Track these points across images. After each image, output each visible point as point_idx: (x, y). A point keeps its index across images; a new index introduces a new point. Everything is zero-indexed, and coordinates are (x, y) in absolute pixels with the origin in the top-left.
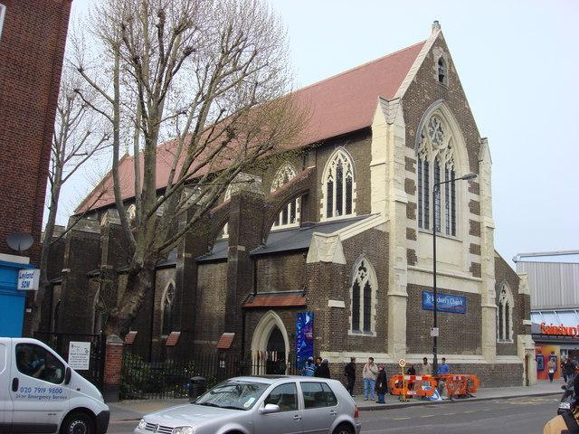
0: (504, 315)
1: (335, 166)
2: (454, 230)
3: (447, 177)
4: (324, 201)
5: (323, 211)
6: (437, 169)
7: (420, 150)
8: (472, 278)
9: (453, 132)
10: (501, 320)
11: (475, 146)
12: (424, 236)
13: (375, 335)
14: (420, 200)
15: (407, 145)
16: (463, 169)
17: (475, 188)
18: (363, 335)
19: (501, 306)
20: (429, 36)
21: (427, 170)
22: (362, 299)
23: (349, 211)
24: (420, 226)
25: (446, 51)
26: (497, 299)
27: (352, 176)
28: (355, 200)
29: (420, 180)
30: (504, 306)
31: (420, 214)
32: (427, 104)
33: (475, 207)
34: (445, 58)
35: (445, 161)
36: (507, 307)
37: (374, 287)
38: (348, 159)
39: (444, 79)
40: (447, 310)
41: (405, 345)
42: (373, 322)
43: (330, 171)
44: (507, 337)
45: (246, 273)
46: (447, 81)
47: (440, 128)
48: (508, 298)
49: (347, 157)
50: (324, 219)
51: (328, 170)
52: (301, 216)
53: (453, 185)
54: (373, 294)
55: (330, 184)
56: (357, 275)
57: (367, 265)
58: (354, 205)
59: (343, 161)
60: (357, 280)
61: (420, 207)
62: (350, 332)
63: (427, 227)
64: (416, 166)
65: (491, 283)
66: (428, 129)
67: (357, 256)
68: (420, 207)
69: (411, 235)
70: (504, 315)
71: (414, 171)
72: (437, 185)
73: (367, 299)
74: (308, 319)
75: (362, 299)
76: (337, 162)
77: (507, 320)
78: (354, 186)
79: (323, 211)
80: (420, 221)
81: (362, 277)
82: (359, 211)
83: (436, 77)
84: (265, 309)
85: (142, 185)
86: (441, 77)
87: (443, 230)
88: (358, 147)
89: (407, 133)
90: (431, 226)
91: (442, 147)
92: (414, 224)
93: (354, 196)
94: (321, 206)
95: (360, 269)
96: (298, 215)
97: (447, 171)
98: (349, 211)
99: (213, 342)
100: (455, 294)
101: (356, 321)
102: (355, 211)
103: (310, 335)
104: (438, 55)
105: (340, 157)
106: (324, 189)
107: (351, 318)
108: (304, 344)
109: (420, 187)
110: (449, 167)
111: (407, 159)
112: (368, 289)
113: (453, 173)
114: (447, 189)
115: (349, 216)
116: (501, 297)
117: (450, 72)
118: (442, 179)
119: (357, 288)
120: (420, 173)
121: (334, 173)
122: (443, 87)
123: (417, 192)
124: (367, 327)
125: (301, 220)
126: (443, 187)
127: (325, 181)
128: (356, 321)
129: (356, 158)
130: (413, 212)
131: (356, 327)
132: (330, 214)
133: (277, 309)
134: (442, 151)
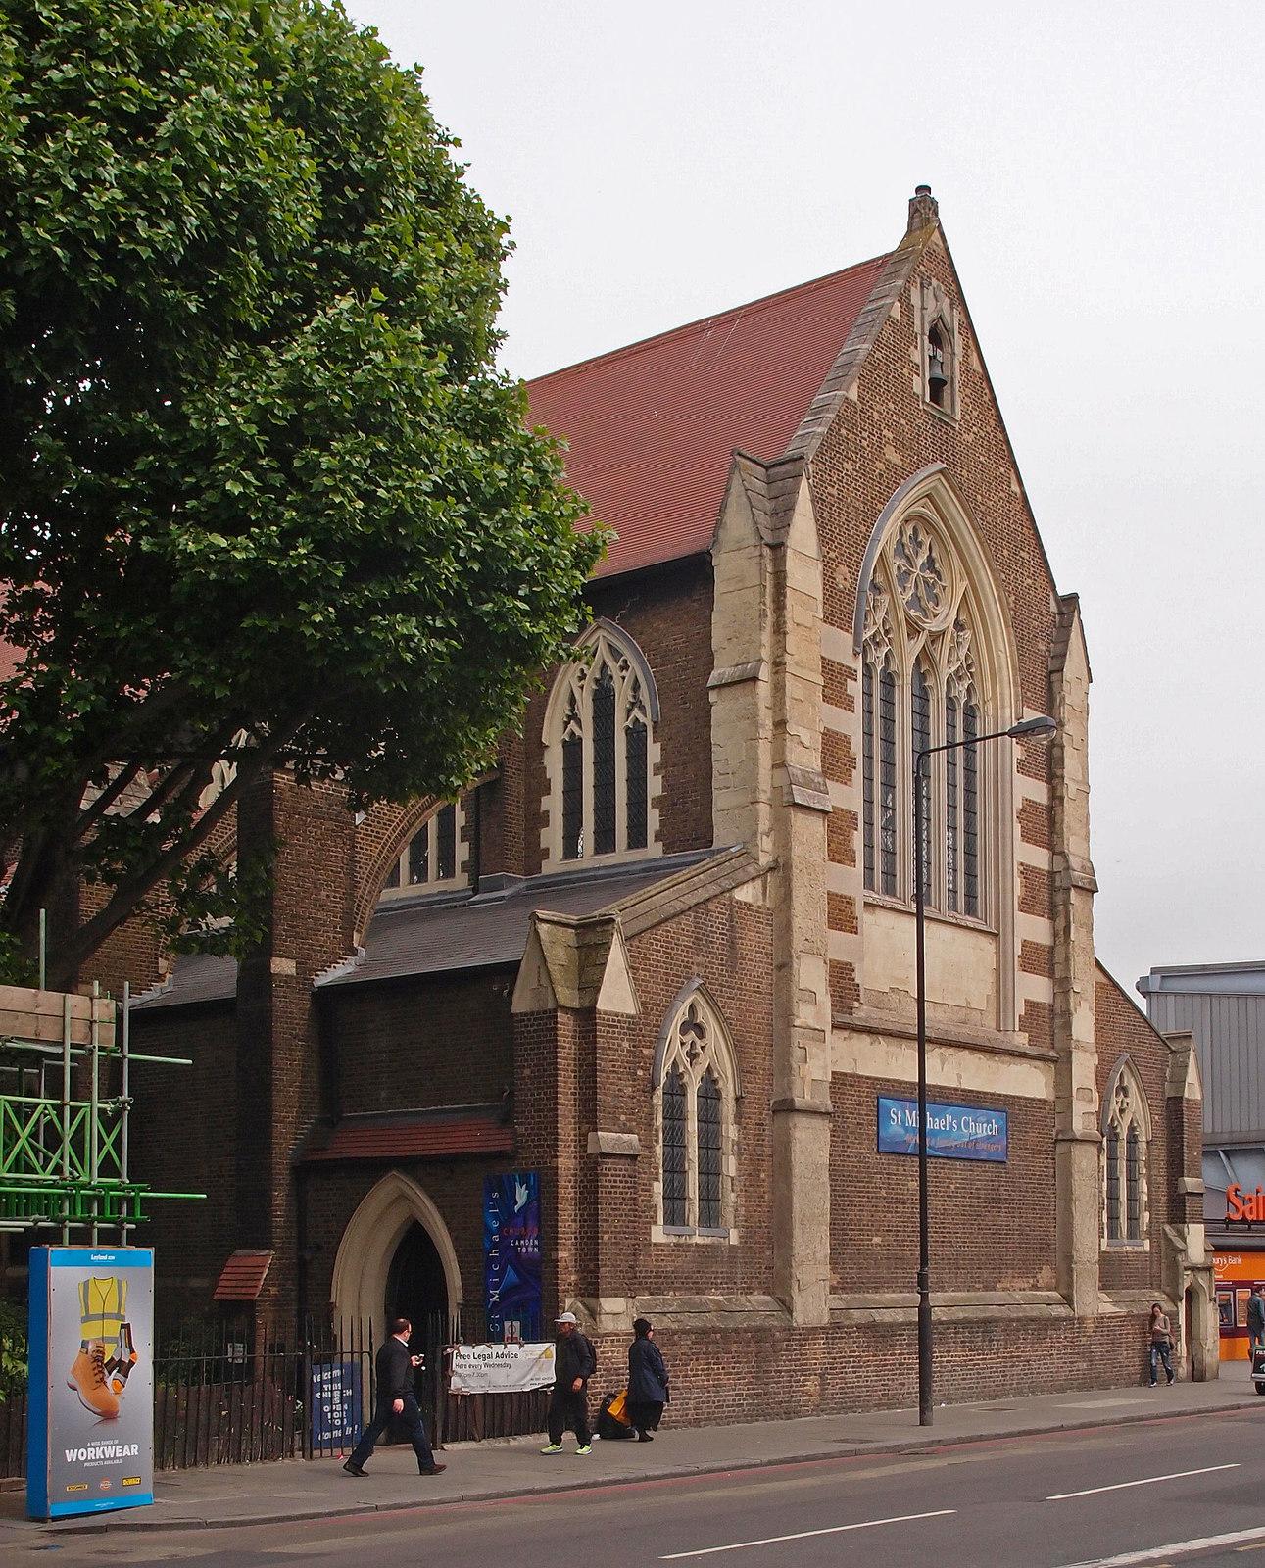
0: (1122, 1166)
1: (590, 686)
2: (971, 895)
3: (951, 726)
4: (554, 803)
5: (553, 836)
6: (922, 696)
7: (867, 635)
8: (1016, 898)
9: (974, 574)
10: (1113, 1178)
11: (1051, 627)
12: (884, 919)
13: (734, 1238)
14: (869, 801)
15: (828, 619)
16: (1005, 704)
17: (1050, 767)
18: (697, 1239)
19: (1114, 1138)
20: (886, 234)
21: (888, 702)
22: (692, 1126)
23: (637, 839)
24: (869, 884)
25: (959, 299)
26: (1102, 1114)
27: (647, 721)
28: (658, 802)
29: (868, 734)
30: (1124, 1134)
31: (869, 846)
32: (897, 476)
33: (1048, 824)
34: (954, 319)
35: (946, 671)
36: (1132, 1139)
37: (728, 1089)
38: (633, 663)
39: (947, 391)
40: (951, 1157)
41: (825, 1271)
42: (730, 1198)
43: (573, 701)
44: (1132, 1235)
45: (649, 1223)
46: (958, 403)
47: (931, 560)
48: (1137, 1112)
49: (628, 655)
50: (554, 864)
51: (564, 696)
52: (476, 851)
53: (970, 751)
54: (728, 1108)
55: (572, 747)
56: (674, 1046)
57: (706, 1016)
58: (654, 819)
59: (614, 667)
60: (675, 1065)
61: (869, 824)
62: (658, 1234)
63: (889, 889)
64: (855, 688)
65: (1084, 1069)
66: (895, 563)
67: (675, 991)
68: (869, 824)
69: (841, 915)
70: (1122, 1166)
71: (850, 708)
72: (922, 755)
73: (710, 1119)
74: (522, 1195)
75: (692, 1126)
76: (593, 672)
77: (1132, 1180)
78: (654, 753)
79: (553, 836)
80: (869, 869)
81: (693, 1056)
82: (671, 839)
83: (920, 386)
84: (373, 1169)
85: (1243, 1549)
86: (937, 386)
87: (939, 893)
88: (668, 627)
89: (828, 579)
90: (906, 883)
91: (932, 625)
92: (850, 880)
93: (655, 786)
94: (543, 820)
95: (685, 1029)
96: (462, 852)
97: (951, 707)
98: (637, 839)
99: (195, 1283)
100: (974, 1101)
101: (675, 1196)
102: (658, 837)
103: (529, 1246)
104: (928, 305)
105: (603, 652)
106: (554, 764)
107: (658, 1187)
108: (511, 1275)
109: (868, 757)
110: (960, 690)
111: (828, 667)
112: (710, 1093)
113: (970, 713)
114: (952, 764)
115: (637, 855)
116: (1115, 1107)
117: (967, 371)
118: (938, 735)
119: (676, 1089)
120: (868, 712)
121: (586, 711)
122: (942, 423)
123: (858, 775)
124: (710, 1216)
125: (474, 868)
126: (938, 762)
127: (553, 735)
128: (675, 1196)
129: (658, 658)
130: (848, 839)
131: (675, 1217)
132: (571, 851)
133: (409, 1165)
134: (936, 637)
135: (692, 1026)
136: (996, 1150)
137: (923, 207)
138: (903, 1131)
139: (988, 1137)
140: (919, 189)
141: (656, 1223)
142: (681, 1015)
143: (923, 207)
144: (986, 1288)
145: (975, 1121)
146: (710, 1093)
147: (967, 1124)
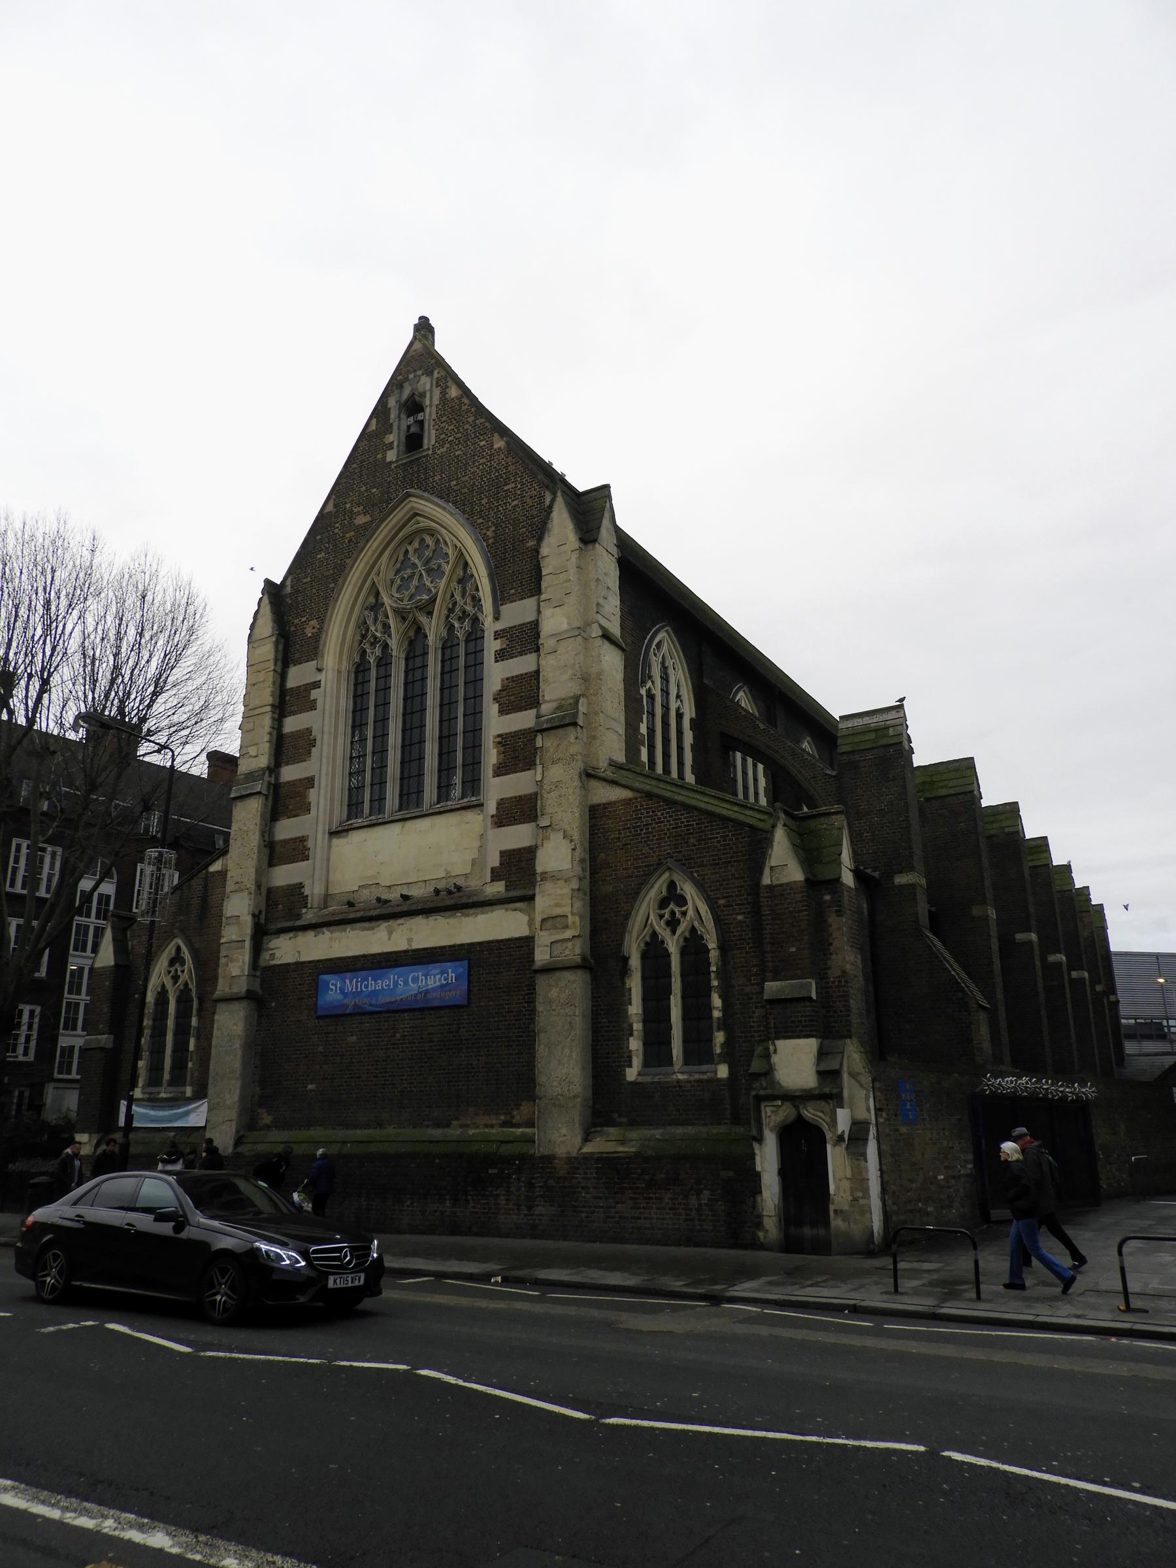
37: (192, 986)
57: (688, 890)
81: (673, 924)
135: (673, 896)
136: (458, 995)
137: (424, 328)
138: (340, 997)
139: (442, 986)
140: (420, 318)
141: (630, 1066)
142: (657, 888)
143: (424, 328)
144: (438, 1125)
145: (426, 976)
146: (693, 946)
147: (415, 980)
